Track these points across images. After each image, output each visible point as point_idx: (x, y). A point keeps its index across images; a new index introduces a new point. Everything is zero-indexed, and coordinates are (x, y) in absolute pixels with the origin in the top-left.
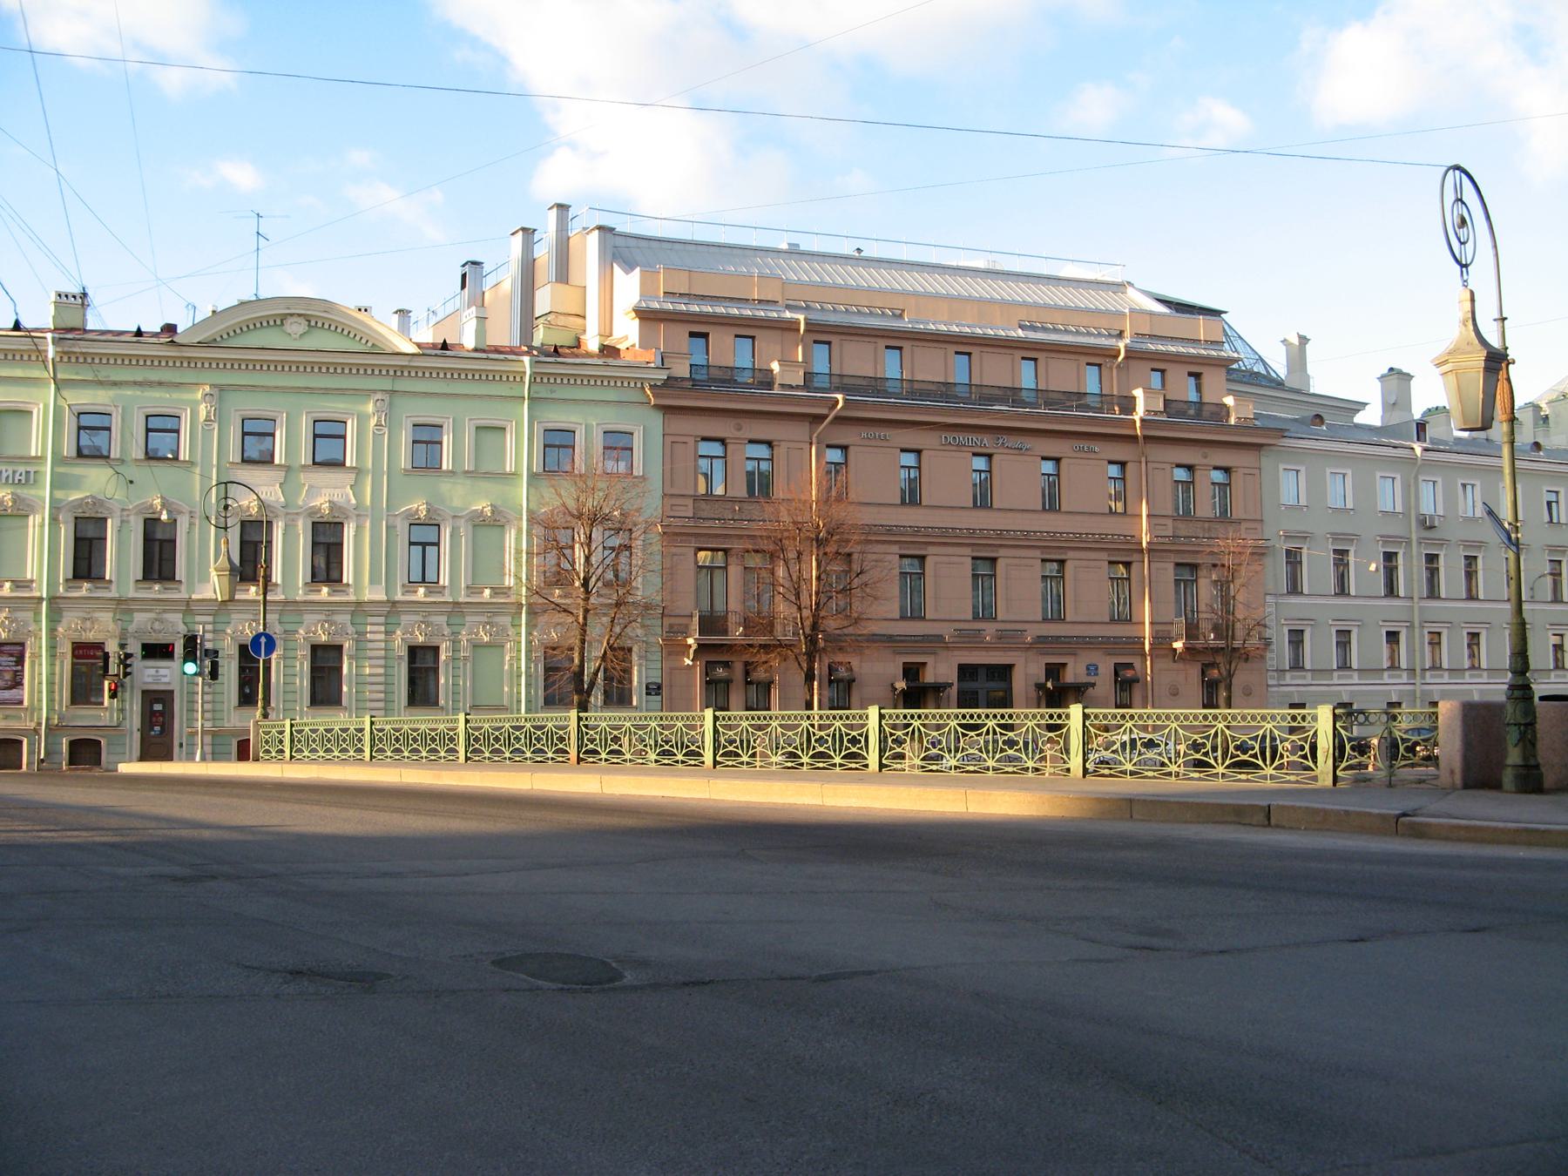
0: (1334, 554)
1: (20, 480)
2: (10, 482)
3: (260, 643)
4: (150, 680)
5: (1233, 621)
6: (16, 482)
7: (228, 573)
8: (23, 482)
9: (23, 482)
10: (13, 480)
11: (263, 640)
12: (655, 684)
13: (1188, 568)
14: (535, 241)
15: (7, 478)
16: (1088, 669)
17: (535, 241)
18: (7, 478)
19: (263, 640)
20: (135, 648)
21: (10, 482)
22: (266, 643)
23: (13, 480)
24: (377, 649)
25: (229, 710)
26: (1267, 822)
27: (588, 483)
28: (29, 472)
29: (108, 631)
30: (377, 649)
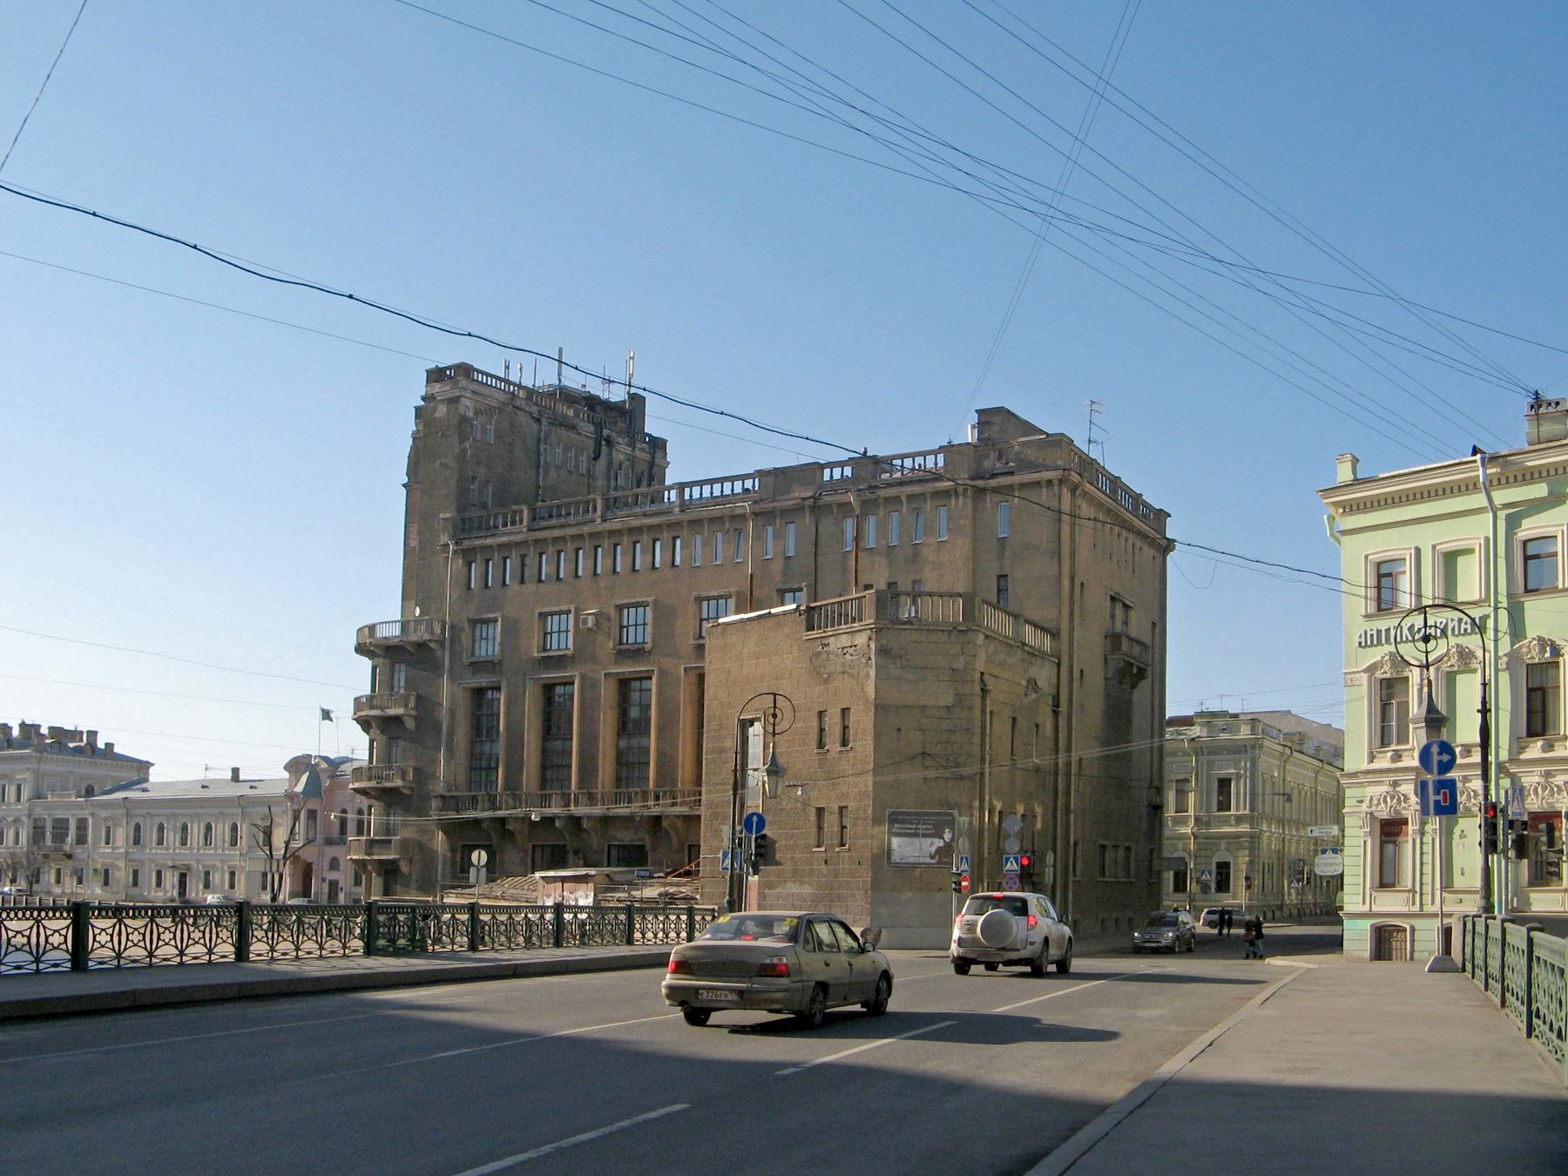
0: (1389, 744)
1: (1466, 630)
2: (1457, 632)
3: (753, 822)
5: (682, 967)
6: (1462, 632)
7: (1424, 724)
8: (1469, 631)
9: (1469, 631)
10: (1459, 631)
11: (755, 819)
13: (1057, 573)
14: (707, 1024)
15: (1453, 629)
17: (707, 1024)
18: (1453, 629)
19: (755, 819)
21: (1457, 632)
22: (757, 822)
23: (1459, 631)
24: (278, 866)
26: (1475, 919)
27: (1165, 541)
28: (1381, 631)
29: (1280, 765)
30: (278, 866)
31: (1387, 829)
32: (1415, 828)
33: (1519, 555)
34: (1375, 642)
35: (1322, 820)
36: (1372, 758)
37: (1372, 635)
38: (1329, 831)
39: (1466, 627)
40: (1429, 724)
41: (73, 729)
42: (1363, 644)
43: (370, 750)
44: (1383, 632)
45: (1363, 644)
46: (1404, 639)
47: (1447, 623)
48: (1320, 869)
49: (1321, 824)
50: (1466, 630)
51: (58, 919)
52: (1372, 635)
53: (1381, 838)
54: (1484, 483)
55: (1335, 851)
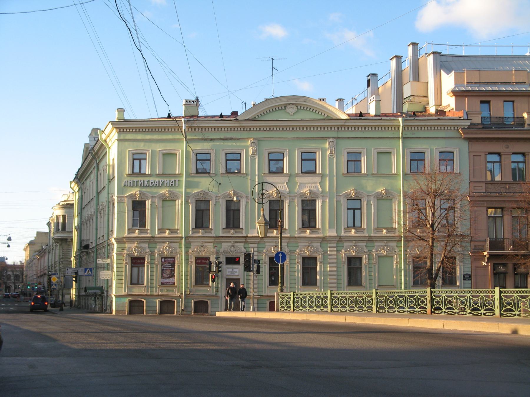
1: (172, 185)
4: (230, 274)
6: (170, 185)
8: (173, 185)
10: (169, 185)
12: (468, 274)
16: (464, 277)
20: (223, 259)
23: (169, 185)
25: (265, 288)
31: (134, 261)
32: (148, 261)
33: (419, 147)
34: (132, 186)
35: (68, 254)
36: (130, 231)
37: (130, 183)
38: (106, 261)
39: (172, 183)
40: (266, 224)
41: (13, 264)
42: (158, 185)
43: (283, 333)
44: (136, 182)
45: (158, 185)
46: (145, 186)
47: (164, 181)
48: (103, 277)
49: (70, 256)
50: (156, 185)
51: (272, 112)
52: (130, 183)
53: (131, 265)
54: (185, 130)
55: (108, 269)
